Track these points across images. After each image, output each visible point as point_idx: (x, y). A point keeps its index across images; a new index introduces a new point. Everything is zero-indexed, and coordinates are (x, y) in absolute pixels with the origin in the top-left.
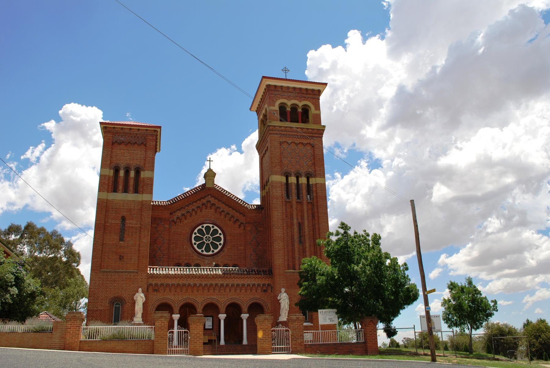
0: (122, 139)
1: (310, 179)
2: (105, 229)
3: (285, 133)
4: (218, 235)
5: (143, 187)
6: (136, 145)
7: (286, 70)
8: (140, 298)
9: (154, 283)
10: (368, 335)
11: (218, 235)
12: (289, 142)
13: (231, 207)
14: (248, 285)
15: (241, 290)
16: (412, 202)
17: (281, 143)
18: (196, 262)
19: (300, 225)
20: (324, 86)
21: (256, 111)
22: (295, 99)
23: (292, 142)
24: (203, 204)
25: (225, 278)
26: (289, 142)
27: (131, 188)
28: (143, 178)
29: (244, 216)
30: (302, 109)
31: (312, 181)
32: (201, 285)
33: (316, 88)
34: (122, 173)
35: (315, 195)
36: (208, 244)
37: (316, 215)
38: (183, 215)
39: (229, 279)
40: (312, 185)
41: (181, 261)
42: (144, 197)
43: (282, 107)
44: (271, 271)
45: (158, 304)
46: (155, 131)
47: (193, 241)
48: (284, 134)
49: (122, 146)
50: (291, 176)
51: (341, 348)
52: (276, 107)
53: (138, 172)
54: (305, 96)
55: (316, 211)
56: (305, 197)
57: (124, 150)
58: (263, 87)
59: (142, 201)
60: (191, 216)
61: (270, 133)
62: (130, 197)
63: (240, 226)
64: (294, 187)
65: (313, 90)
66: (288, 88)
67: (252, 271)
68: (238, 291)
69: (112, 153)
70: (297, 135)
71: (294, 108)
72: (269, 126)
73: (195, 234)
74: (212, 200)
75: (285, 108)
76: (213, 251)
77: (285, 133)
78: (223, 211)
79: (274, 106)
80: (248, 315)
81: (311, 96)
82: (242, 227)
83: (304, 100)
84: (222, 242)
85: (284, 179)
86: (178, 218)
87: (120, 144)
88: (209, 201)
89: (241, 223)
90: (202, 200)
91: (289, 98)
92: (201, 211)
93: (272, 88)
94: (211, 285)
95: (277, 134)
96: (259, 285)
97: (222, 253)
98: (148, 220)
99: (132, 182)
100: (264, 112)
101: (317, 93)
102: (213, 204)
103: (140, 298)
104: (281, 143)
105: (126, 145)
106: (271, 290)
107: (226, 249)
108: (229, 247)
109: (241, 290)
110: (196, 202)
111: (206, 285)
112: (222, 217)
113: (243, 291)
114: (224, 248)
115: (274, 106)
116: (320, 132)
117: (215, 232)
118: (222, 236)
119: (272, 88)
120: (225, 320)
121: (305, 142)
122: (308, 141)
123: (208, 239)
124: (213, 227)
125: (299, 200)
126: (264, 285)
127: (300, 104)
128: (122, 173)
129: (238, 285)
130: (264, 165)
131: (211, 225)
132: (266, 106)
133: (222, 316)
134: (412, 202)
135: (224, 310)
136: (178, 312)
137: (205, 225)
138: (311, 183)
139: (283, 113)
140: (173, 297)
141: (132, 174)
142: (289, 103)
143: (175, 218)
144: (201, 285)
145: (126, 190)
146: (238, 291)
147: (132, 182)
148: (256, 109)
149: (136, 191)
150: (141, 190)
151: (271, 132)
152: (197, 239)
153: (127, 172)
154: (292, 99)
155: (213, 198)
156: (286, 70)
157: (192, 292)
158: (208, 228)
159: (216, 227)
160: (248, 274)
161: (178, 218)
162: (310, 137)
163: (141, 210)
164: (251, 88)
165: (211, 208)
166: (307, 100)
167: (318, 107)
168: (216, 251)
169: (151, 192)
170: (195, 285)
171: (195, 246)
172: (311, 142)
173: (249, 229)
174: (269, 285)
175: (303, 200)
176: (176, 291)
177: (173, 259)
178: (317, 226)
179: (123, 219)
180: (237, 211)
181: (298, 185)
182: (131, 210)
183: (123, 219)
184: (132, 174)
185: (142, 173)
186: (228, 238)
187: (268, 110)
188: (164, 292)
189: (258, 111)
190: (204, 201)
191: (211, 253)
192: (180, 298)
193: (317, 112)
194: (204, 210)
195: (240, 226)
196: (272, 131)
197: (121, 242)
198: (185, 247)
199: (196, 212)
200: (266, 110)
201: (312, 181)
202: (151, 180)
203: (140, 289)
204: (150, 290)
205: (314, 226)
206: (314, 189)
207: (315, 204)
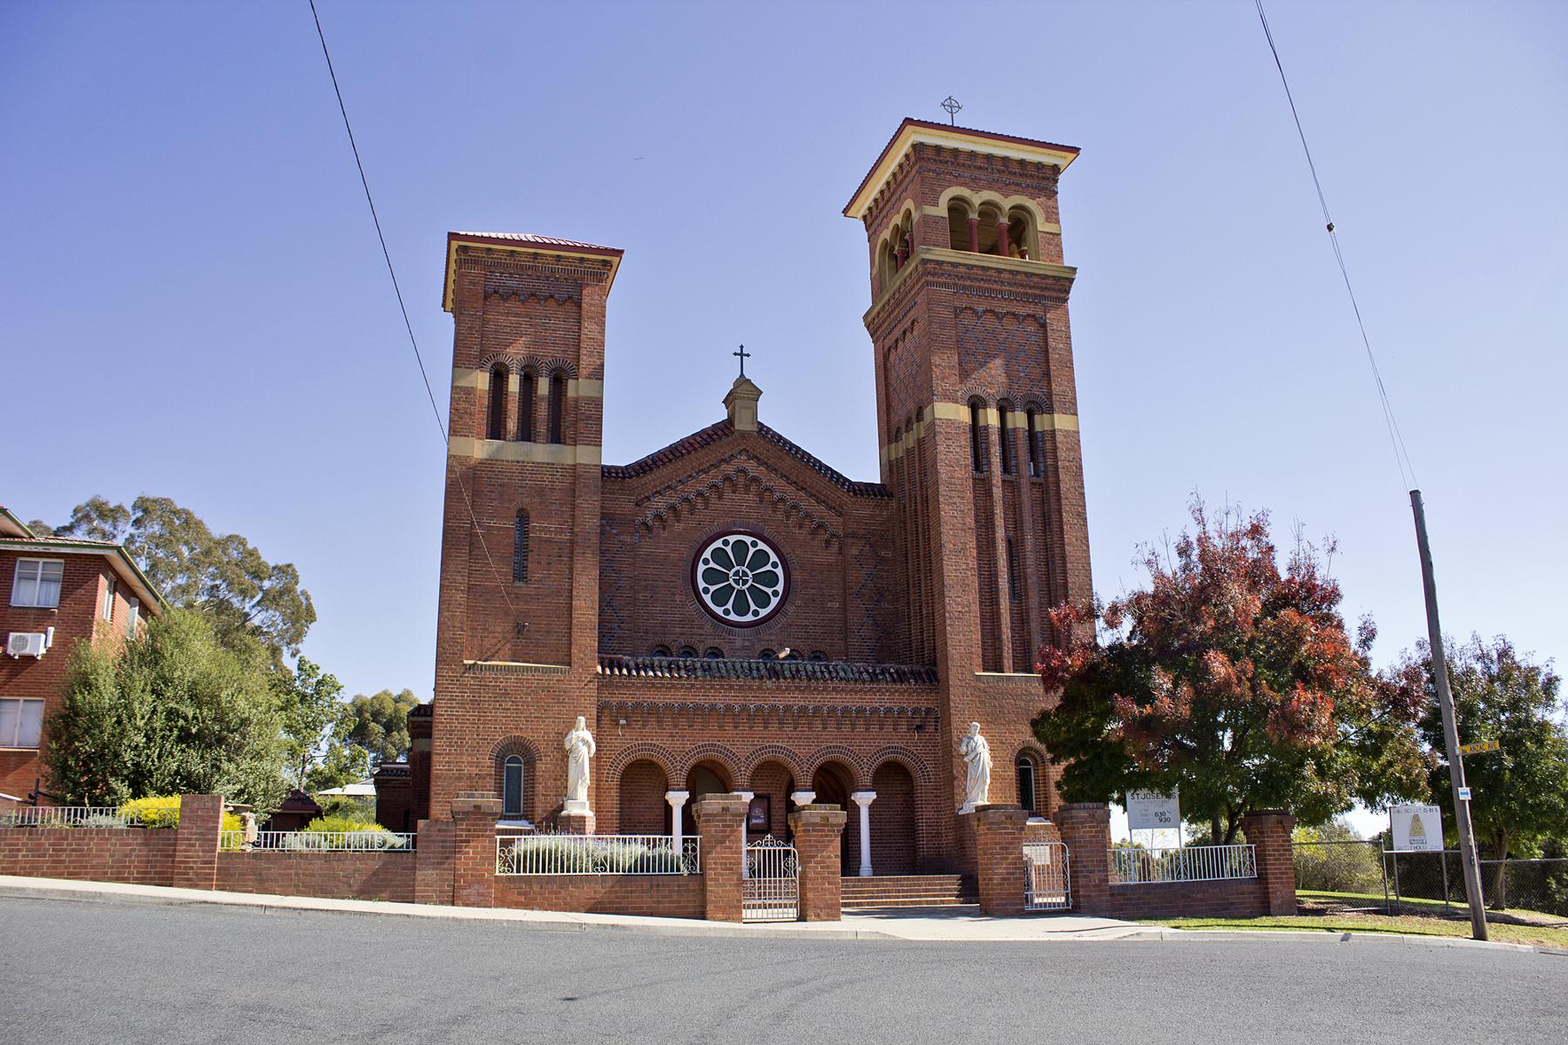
0: (513, 283)
1: (1037, 418)
2: (471, 544)
3: (968, 283)
4: (769, 567)
5: (575, 423)
6: (551, 302)
7: (951, 105)
8: (582, 740)
9: (615, 700)
10: (1270, 860)
11: (769, 567)
12: (980, 309)
13: (803, 489)
14: (874, 711)
15: (853, 726)
16: (1415, 495)
17: (958, 312)
18: (710, 642)
19: (1013, 546)
20: (1072, 156)
21: (864, 218)
22: (991, 188)
23: (987, 311)
24: (727, 478)
25: (812, 692)
26: (980, 309)
27: (542, 428)
28: (576, 400)
29: (841, 515)
30: (1010, 218)
31: (1041, 423)
32: (744, 708)
33: (1047, 158)
34: (514, 383)
35: (1050, 462)
36: (741, 592)
37: (1054, 517)
38: (672, 508)
39: (820, 692)
40: (1015, 430)
41: (668, 640)
42: (581, 455)
43: (958, 208)
44: (935, 674)
45: (627, 761)
46: (605, 263)
47: (701, 584)
48: (964, 287)
49: (512, 305)
50: (985, 407)
51: (1200, 896)
52: (942, 210)
53: (558, 382)
54: (1019, 180)
55: (1054, 506)
56: (1023, 467)
57: (517, 315)
58: (903, 148)
59: (575, 466)
60: (692, 511)
61: (928, 283)
62: (541, 452)
63: (828, 542)
64: (995, 438)
65: (1039, 166)
66: (973, 154)
67: (883, 673)
68: (846, 729)
69: (485, 322)
70: (1001, 292)
71: (989, 210)
72: (925, 262)
73: (706, 562)
74: (752, 468)
75: (965, 212)
76: (756, 613)
77: (968, 283)
78: (781, 500)
79: (937, 205)
80: (873, 795)
81: (1035, 182)
82: (835, 548)
83: (1016, 192)
84: (780, 587)
85: (963, 414)
86: (658, 517)
87: (505, 298)
88: (743, 471)
89: (833, 536)
90: (723, 466)
91: (975, 185)
92: (720, 498)
93: (931, 154)
94: (774, 708)
95: (945, 285)
96: (902, 711)
97: (782, 620)
98: (589, 521)
99: (542, 411)
100: (897, 219)
101: (1049, 173)
102: (755, 479)
103: (582, 740)
104: (958, 312)
105: (523, 302)
106: (935, 724)
107: (790, 608)
108: (799, 603)
109: (853, 726)
110: (705, 472)
111: (759, 709)
112: (780, 516)
113: (860, 728)
114: (787, 606)
115: (937, 205)
116: (1059, 286)
117: (761, 557)
118: (779, 571)
119: (931, 154)
120: (871, 808)
121: (1022, 310)
122: (1030, 310)
123: (741, 578)
124: (754, 544)
125: (1008, 477)
126: (915, 711)
127: (1007, 203)
128: (514, 383)
129: (846, 710)
130: (893, 375)
131: (748, 540)
132: (909, 204)
133: (864, 799)
134: (1415, 495)
135: (867, 781)
136: (683, 784)
137: (732, 539)
138: (1038, 428)
139: (962, 228)
140: (666, 743)
141: (543, 386)
142: (977, 199)
143: (650, 514)
144: (744, 708)
145: (526, 433)
146: (846, 729)
147: (542, 411)
148: (863, 211)
149: (556, 437)
150: (570, 433)
151: (930, 278)
152: (710, 576)
153: (528, 380)
154: (984, 188)
155: (723, 466)
156: (951, 105)
157: (721, 727)
158: (740, 548)
159: (762, 546)
160: (872, 681)
161: (658, 517)
162: (1036, 296)
163: (573, 490)
164: (858, 150)
165: (747, 489)
166: (1023, 193)
167: (1052, 215)
168: (763, 612)
169: (598, 443)
170: (729, 708)
171: (707, 598)
172: (1039, 311)
173: (855, 552)
174: (928, 711)
175: (1019, 476)
176: (675, 726)
177: (646, 632)
178: (1057, 551)
179: (523, 517)
180: (819, 501)
181: (977, 431)
182: (542, 489)
183: (523, 517)
184: (543, 386)
185: (571, 383)
186: (797, 576)
187: (915, 216)
188: (644, 726)
189: (872, 220)
190: (729, 469)
191: (749, 618)
192: (688, 747)
193: (1051, 228)
194: (728, 495)
195: (828, 542)
196: (933, 275)
197: (518, 584)
198: (677, 598)
199: (706, 500)
200: (908, 214)
201: (1041, 423)
202: (598, 403)
203: (582, 719)
204: (606, 721)
205: (1047, 548)
206: (1049, 445)
207: (1052, 487)
